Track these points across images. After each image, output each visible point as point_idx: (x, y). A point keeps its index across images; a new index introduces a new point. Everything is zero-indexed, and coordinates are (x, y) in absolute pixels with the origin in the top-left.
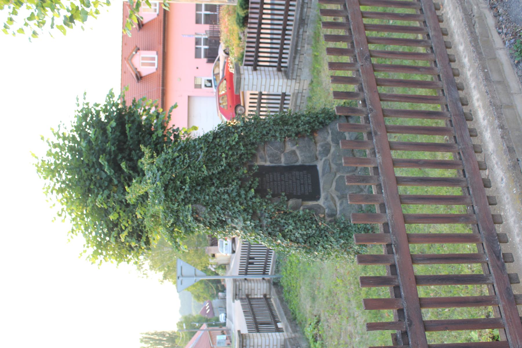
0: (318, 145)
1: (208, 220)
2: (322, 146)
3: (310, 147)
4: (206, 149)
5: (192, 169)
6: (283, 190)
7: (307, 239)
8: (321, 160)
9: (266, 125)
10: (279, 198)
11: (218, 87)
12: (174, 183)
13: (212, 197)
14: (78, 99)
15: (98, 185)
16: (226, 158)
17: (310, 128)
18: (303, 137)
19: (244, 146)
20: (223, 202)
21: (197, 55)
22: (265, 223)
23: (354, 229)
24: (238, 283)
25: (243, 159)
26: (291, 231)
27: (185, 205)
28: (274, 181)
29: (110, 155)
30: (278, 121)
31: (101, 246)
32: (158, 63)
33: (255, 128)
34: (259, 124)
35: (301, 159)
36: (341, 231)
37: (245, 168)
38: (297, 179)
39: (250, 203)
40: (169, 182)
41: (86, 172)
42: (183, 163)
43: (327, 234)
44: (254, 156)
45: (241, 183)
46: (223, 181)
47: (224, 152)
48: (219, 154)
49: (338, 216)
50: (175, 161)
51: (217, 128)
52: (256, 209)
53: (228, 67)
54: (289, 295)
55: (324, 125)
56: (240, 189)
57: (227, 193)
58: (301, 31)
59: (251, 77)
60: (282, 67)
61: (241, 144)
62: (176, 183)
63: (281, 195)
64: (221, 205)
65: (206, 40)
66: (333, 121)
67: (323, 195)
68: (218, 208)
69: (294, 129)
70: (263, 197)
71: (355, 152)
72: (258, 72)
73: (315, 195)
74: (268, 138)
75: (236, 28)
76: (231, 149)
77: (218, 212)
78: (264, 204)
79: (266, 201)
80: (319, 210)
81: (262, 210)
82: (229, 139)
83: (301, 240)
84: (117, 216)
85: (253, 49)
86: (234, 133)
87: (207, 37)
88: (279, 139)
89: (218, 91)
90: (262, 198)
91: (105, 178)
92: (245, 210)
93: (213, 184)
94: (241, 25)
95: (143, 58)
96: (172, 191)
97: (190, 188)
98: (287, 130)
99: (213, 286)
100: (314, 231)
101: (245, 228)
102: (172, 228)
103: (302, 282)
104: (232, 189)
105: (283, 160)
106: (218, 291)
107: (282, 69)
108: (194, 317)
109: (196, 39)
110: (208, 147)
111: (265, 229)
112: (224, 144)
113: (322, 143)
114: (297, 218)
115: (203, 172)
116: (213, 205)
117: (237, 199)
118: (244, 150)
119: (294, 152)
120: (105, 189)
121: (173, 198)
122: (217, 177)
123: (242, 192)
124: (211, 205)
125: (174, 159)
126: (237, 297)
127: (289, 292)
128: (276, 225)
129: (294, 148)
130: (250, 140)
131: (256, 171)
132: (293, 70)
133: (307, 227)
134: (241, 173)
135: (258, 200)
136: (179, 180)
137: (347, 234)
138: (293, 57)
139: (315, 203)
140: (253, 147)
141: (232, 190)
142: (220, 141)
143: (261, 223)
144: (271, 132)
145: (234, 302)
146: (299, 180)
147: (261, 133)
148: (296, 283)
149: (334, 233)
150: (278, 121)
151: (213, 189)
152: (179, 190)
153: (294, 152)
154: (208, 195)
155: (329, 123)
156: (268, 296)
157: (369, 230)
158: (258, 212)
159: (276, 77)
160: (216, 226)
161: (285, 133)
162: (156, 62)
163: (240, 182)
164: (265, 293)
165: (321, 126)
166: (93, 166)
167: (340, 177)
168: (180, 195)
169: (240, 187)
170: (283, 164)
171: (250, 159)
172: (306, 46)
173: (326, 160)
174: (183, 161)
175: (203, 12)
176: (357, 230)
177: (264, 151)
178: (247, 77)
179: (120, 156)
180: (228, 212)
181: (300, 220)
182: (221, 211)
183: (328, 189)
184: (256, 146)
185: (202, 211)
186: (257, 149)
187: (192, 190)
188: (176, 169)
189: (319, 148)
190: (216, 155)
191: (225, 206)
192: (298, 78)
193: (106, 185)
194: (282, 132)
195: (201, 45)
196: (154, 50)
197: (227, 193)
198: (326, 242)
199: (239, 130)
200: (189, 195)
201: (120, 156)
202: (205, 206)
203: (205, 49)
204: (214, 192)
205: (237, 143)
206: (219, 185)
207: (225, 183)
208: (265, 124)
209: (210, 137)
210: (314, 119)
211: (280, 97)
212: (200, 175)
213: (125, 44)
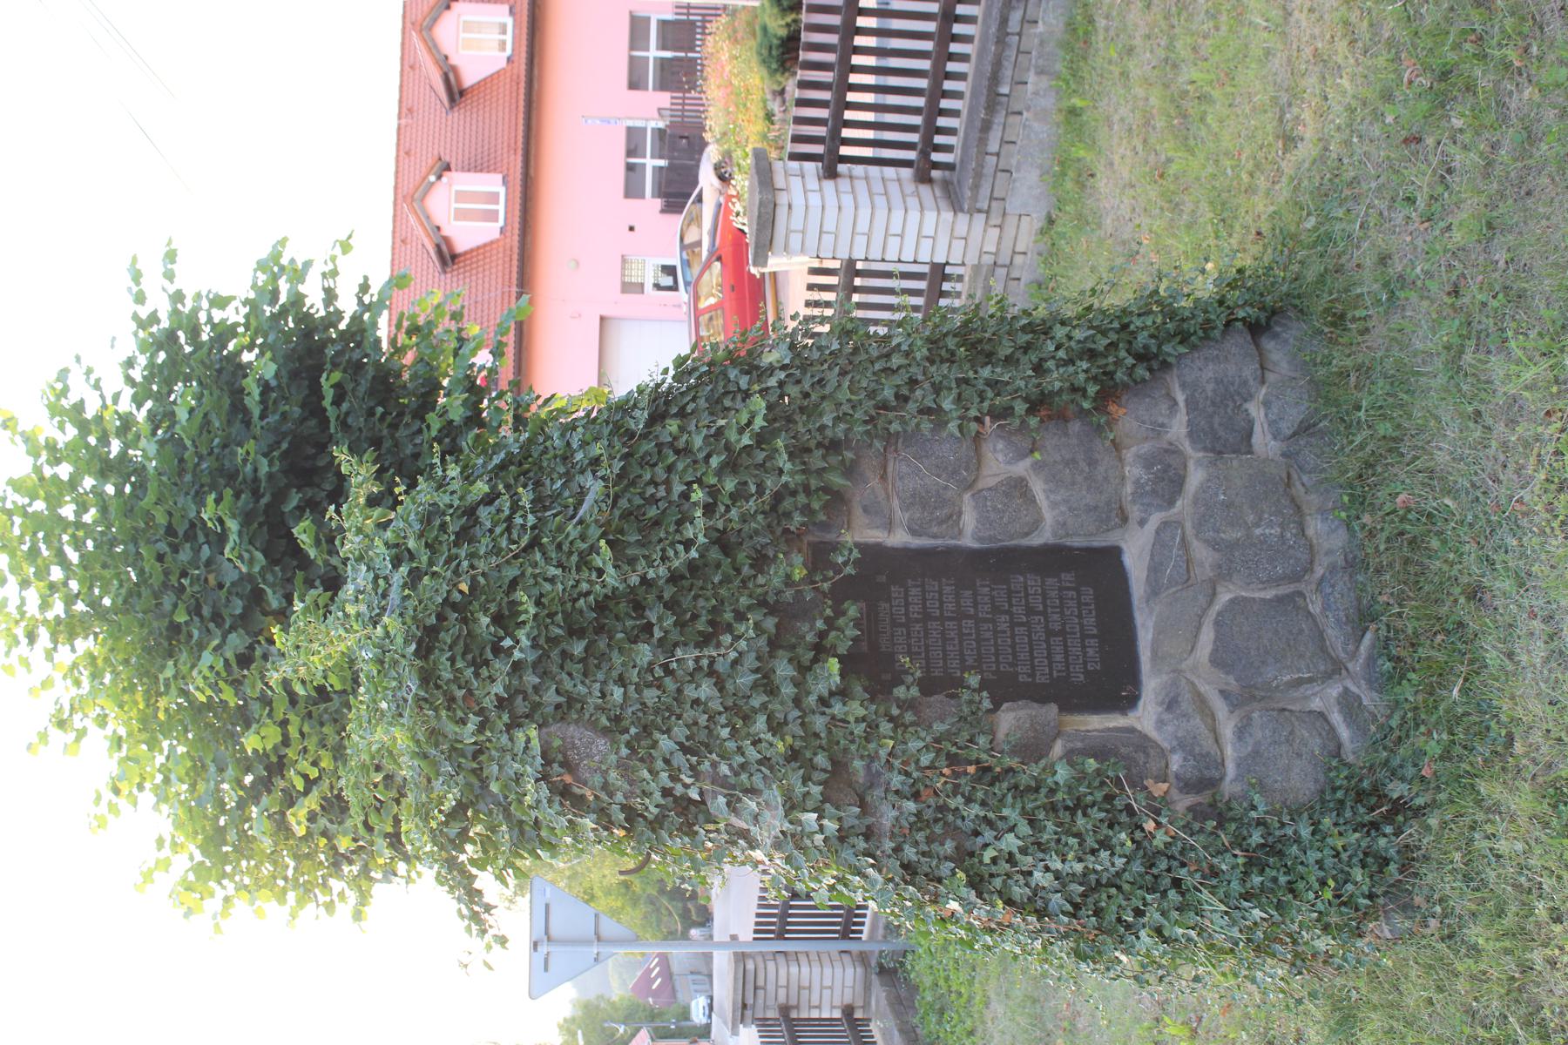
0: (1129, 455)
1: (619, 797)
2: (1148, 462)
3: (1092, 463)
4: (618, 466)
5: (547, 560)
6: (970, 662)
7: (1084, 895)
8: (1142, 523)
9: (896, 361)
10: (952, 696)
11: (694, 287)
12: (465, 621)
13: (638, 690)
14: (137, 277)
15: (206, 611)
16: (709, 510)
17: (1095, 379)
18: (1061, 417)
19: (791, 456)
20: (689, 714)
21: (632, 190)
22: (887, 816)
23: (1313, 856)
24: (750, 966)
25: (788, 515)
26: (1011, 859)
27: (509, 728)
28: (927, 617)
29: (256, 494)
30: (951, 343)
31: (222, 844)
32: (506, 212)
33: (843, 373)
34: (864, 356)
35: (1051, 518)
36: (1254, 863)
37: (798, 559)
38: (1030, 611)
39: (819, 723)
40: (441, 617)
41: (160, 558)
42: (508, 530)
43: (1183, 873)
44: (837, 500)
45: (777, 626)
46: (695, 617)
47: (699, 481)
48: (678, 488)
49: (1229, 787)
50: (477, 522)
51: (672, 372)
52: (846, 750)
53: (728, 211)
54: (939, 1023)
55: (1155, 364)
56: (772, 655)
57: (712, 672)
58: (1015, 17)
59: (815, 200)
60: (936, 166)
61: (780, 443)
62: (476, 621)
63: (961, 683)
64: (680, 732)
65: (660, 133)
66: (1194, 347)
67: (1151, 685)
68: (666, 744)
69: (1021, 379)
70: (879, 690)
71: (1298, 490)
72: (844, 184)
73: (1115, 684)
74: (903, 422)
75: (756, 80)
76: (731, 466)
77: (667, 761)
78: (885, 727)
79: (895, 712)
80: (1141, 758)
81: (872, 758)
82: (722, 422)
83: (1057, 900)
84: (273, 735)
85: (823, 113)
86: (747, 395)
87: (661, 125)
88: (953, 427)
89: (697, 298)
90: (872, 700)
91: (233, 584)
92: (793, 755)
93: (648, 628)
94: (774, 66)
95: (462, 196)
96: (452, 660)
97: (535, 646)
98: (992, 384)
99: (674, 908)
100: (1120, 862)
101: (792, 841)
102: (453, 831)
103: (993, 983)
104: (733, 655)
105: (969, 520)
106: (689, 923)
107: (935, 174)
108: (613, 1004)
109: (630, 130)
110: (625, 457)
111: (888, 845)
112: (698, 441)
113: (1146, 448)
114: (1042, 798)
115: (600, 572)
116: (646, 730)
117: (756, 702)
118: (792, 473)
119: (1018, 486)
120: (233, 628)
121: (460, 693)
122: (667, 596)
123: (783, 670)
124: (633, 730)
125: (471, 512)
126: (749, 1013)
127: (941, 1012)
128: (938, 829)
129: (1022, 468)
130: (822, 428)
131: (849, 570)
132: (978, 175)
133: (1091, 842)
134: (777, 582)
135: (856, 709)
136: (486, 611)
137: (1283, 879)
138: (978, 124)
139: (1115, 721)
140: (834, 460)
141: (735, 663)
142: (682, 429)
143: (870, 820)
144: (919, 393)
145: (735, 1032)
146: (1044, 613)
147: (872, 394)
148: (971, 982)
149: (1215, 873)
150: (951, 343)
151: (644, 653)
152: (490, 656)
153: (1018, 486)
154: (622, 681)
155: (1180, 356)
156: (858, 1014)
157: (1386, 861)
158: (858, 764)
159: (913, 202)
160: (656, 824)
161: (982, 396)
162: (501, 207)
163: (770, 623)
164: (848, 1000)
165: (1141, 372)
166: (190, 536)
167: (1232, 601)
168: (492, 680)
169: (774, 644)
170: (968, 541)
171: (822, 517)
172: (1031, 78)
173: (1165, 524)
174: (509, 519)
175: (654, 53)
176: (1329, 862)
177: (883, 477)
178: (798, 201)
179: (294, 499)
180: (714, 765)
181: (1052, 808)
182: (679, 759)
183: (1177, 662)
184: (849, 455)
185: (590, 756)
186: (850, 471)
187: (546, 655)
188: (472, 556)
189: (1133, 471)
190: (662, 492)
191: (702, 736)
192: (993, 209)
193: (238, 611)
194: (968, 392)
195: (644, 157)
196: (495, 170)
197: (712, 672)
198: (1175, 914)
199: (772, 382)
200: (531, 679)
201: (294, 499)
202: (605, 732)
204: (650, 670)
205: (761, 439)
206: (675, 636)
207: (701, 625)
208: (888, 356)
209: (637, 413)
210: (1113, 337)
211: (922, 285)
212: (585, 586)
213: (404, 152)
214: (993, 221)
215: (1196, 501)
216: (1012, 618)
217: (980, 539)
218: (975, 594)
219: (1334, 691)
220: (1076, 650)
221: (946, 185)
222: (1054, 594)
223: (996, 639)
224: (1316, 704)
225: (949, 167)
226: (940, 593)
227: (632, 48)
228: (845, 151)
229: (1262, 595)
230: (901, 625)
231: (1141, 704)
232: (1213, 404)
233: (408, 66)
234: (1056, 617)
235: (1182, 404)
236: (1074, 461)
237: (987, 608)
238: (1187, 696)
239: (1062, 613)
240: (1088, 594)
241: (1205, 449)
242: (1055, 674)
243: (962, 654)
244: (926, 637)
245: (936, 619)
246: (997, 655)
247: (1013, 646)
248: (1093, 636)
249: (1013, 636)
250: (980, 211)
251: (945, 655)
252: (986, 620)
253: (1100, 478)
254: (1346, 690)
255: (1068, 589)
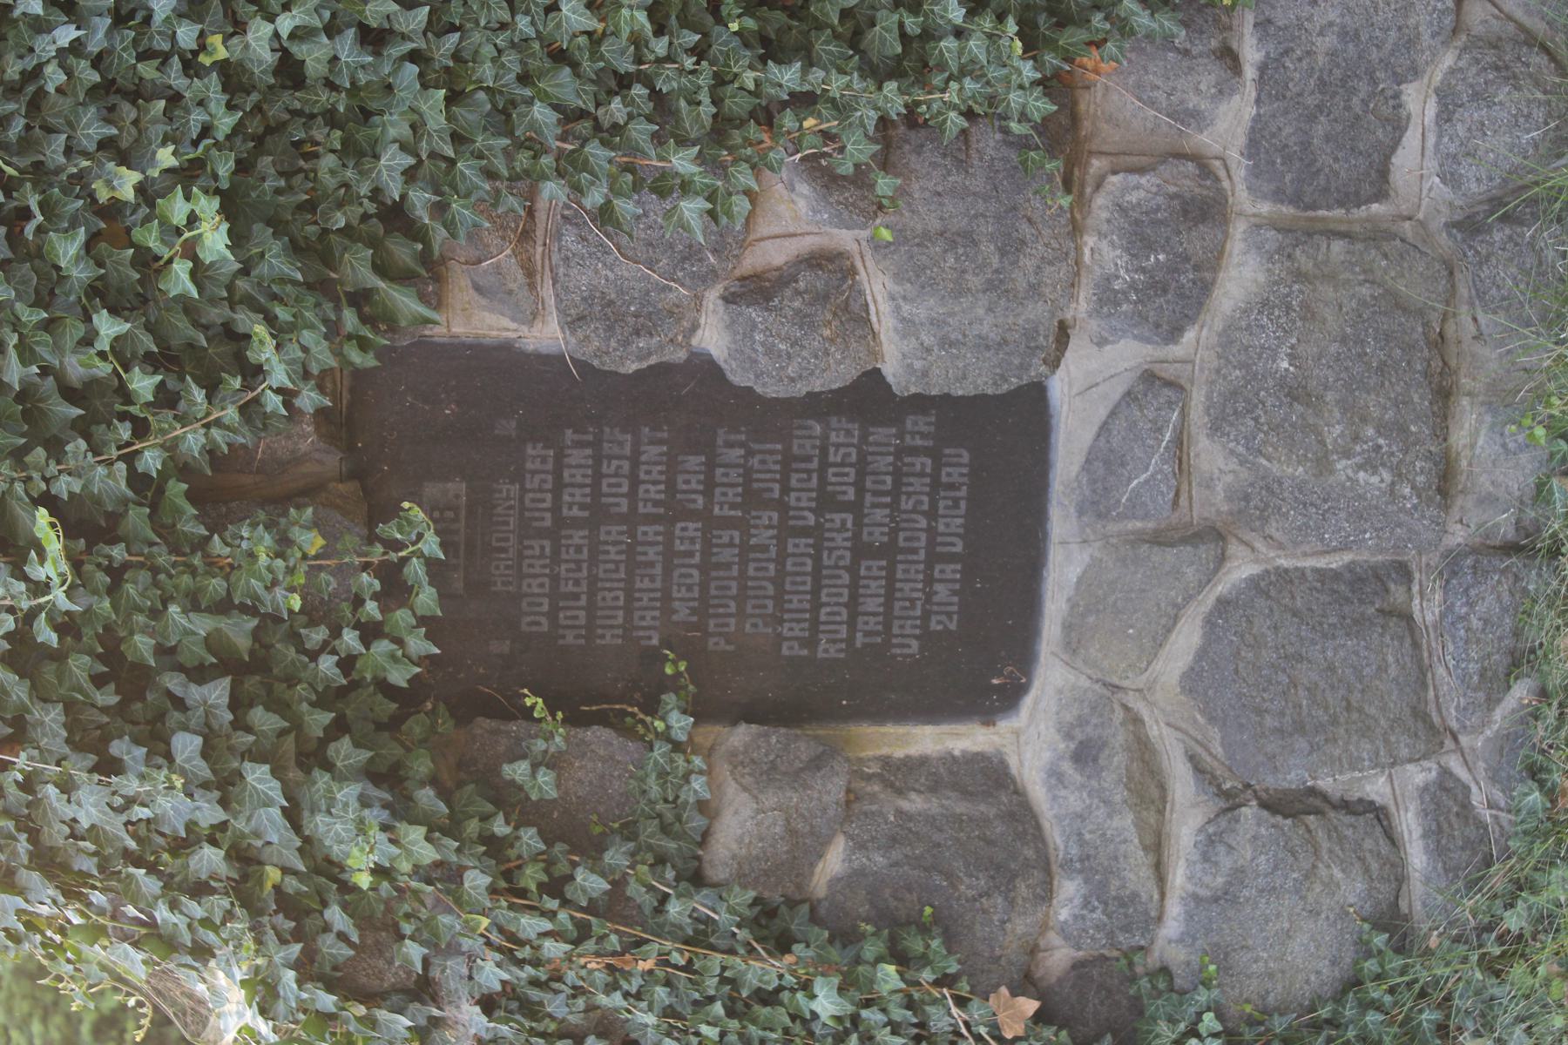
28: (598, 513)
35: (906, 334)
38: (826, 502)
67: (1053, 678)
215: (1227, 339)
216: (784, 517)
219: (1419, 775)
220: (911, 588)
222: (884, 463)
223: (744, 563)
224: (1376, 788)
226: (635, 462)
229: (1321, 563)
230: (541, 534)
231: (1028, 701)
232: (1322, 84)
234: (880, 514)
235: (1250, 73)
236: (969, 238)
238: (1119, 737)
239: (894, 506)
241: (1278, 196)
242: (860, 639)
243: (667, 597)
244: (593, 561)
246: (741, 599)
248: (952, 558)
249: (780, 560)
251: (630, 599)
252: (728, 523)
253: (1021, 284)
254: (1445, 772)
255: (914, 451)
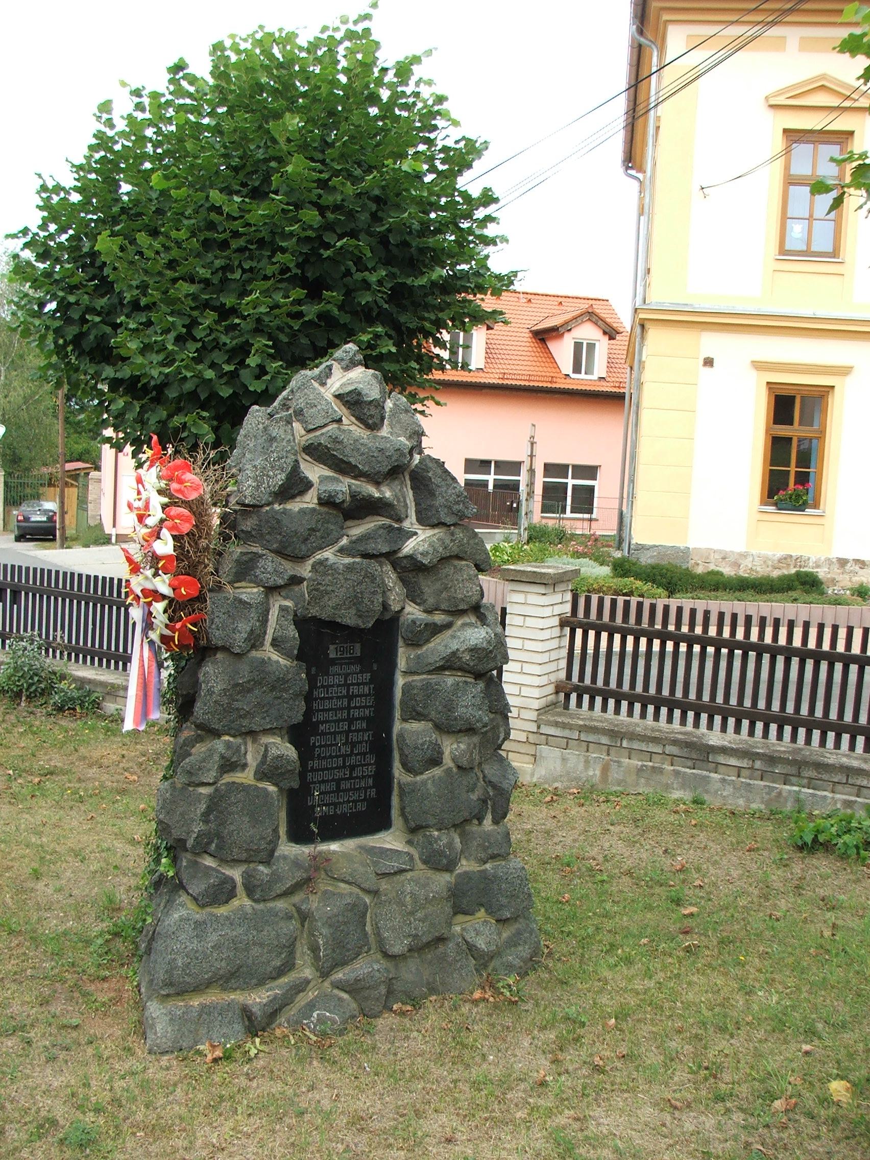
28: (350, 697)
38: (352, 768)
59: (547, 612)
60: (567, 697)
72: (556, 632)
95: (591, 347)
119: (436, 761)
153: (436, 761)
159: (544, 680)
195: (495, 474)
203: (485, 484)
214: (531, 736)
217: (401, 735)
218: (363, 730)
219: (308, 973)
221: (554, 704)
225: (566, 706)
227: (574, 467)
228: (579, 632)
230: (346, 680)
233: (562, 300)
237: (355, 739)
240: (362, 807)
245: (349, 703)
246: (325, 746)
247: (331, 757)
249: (337, 756)
250: (539, 727)
252: (347, 738)
